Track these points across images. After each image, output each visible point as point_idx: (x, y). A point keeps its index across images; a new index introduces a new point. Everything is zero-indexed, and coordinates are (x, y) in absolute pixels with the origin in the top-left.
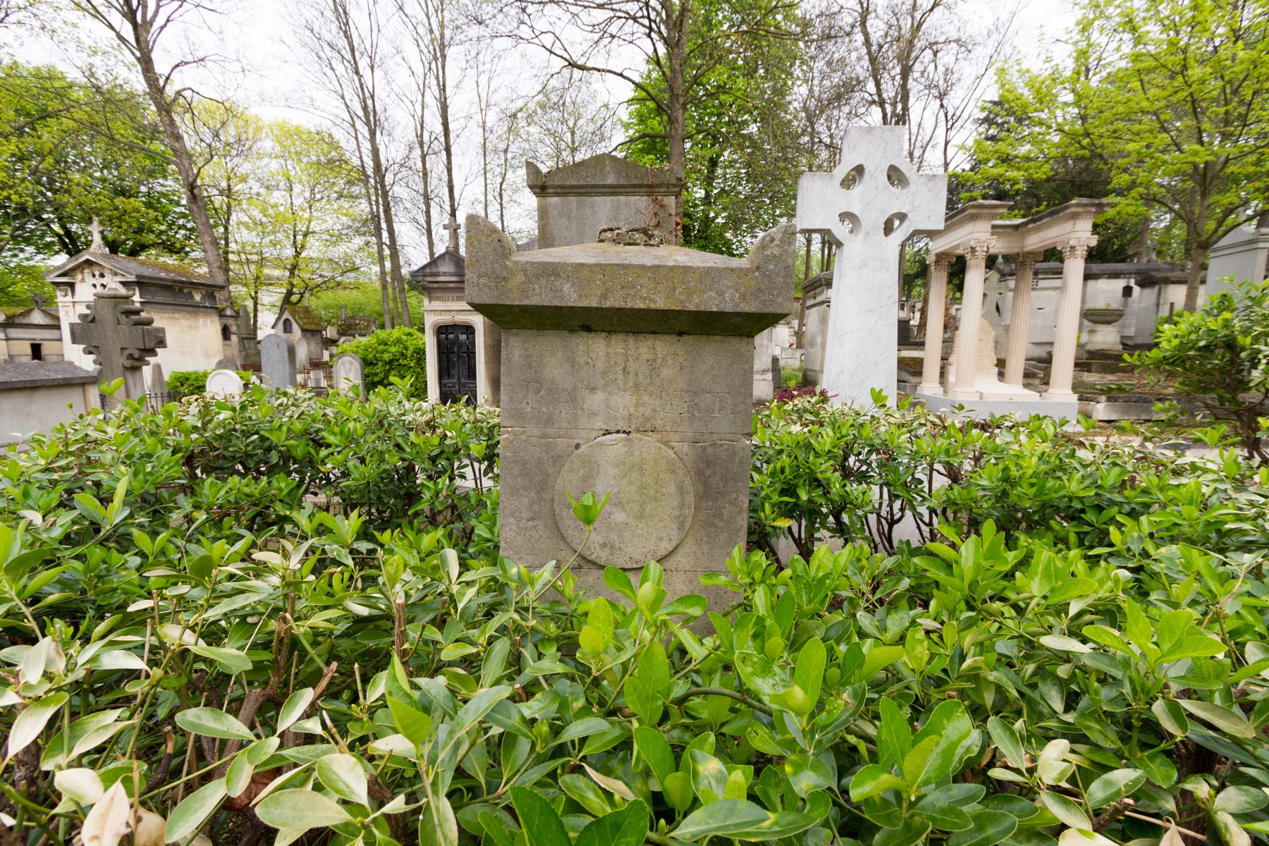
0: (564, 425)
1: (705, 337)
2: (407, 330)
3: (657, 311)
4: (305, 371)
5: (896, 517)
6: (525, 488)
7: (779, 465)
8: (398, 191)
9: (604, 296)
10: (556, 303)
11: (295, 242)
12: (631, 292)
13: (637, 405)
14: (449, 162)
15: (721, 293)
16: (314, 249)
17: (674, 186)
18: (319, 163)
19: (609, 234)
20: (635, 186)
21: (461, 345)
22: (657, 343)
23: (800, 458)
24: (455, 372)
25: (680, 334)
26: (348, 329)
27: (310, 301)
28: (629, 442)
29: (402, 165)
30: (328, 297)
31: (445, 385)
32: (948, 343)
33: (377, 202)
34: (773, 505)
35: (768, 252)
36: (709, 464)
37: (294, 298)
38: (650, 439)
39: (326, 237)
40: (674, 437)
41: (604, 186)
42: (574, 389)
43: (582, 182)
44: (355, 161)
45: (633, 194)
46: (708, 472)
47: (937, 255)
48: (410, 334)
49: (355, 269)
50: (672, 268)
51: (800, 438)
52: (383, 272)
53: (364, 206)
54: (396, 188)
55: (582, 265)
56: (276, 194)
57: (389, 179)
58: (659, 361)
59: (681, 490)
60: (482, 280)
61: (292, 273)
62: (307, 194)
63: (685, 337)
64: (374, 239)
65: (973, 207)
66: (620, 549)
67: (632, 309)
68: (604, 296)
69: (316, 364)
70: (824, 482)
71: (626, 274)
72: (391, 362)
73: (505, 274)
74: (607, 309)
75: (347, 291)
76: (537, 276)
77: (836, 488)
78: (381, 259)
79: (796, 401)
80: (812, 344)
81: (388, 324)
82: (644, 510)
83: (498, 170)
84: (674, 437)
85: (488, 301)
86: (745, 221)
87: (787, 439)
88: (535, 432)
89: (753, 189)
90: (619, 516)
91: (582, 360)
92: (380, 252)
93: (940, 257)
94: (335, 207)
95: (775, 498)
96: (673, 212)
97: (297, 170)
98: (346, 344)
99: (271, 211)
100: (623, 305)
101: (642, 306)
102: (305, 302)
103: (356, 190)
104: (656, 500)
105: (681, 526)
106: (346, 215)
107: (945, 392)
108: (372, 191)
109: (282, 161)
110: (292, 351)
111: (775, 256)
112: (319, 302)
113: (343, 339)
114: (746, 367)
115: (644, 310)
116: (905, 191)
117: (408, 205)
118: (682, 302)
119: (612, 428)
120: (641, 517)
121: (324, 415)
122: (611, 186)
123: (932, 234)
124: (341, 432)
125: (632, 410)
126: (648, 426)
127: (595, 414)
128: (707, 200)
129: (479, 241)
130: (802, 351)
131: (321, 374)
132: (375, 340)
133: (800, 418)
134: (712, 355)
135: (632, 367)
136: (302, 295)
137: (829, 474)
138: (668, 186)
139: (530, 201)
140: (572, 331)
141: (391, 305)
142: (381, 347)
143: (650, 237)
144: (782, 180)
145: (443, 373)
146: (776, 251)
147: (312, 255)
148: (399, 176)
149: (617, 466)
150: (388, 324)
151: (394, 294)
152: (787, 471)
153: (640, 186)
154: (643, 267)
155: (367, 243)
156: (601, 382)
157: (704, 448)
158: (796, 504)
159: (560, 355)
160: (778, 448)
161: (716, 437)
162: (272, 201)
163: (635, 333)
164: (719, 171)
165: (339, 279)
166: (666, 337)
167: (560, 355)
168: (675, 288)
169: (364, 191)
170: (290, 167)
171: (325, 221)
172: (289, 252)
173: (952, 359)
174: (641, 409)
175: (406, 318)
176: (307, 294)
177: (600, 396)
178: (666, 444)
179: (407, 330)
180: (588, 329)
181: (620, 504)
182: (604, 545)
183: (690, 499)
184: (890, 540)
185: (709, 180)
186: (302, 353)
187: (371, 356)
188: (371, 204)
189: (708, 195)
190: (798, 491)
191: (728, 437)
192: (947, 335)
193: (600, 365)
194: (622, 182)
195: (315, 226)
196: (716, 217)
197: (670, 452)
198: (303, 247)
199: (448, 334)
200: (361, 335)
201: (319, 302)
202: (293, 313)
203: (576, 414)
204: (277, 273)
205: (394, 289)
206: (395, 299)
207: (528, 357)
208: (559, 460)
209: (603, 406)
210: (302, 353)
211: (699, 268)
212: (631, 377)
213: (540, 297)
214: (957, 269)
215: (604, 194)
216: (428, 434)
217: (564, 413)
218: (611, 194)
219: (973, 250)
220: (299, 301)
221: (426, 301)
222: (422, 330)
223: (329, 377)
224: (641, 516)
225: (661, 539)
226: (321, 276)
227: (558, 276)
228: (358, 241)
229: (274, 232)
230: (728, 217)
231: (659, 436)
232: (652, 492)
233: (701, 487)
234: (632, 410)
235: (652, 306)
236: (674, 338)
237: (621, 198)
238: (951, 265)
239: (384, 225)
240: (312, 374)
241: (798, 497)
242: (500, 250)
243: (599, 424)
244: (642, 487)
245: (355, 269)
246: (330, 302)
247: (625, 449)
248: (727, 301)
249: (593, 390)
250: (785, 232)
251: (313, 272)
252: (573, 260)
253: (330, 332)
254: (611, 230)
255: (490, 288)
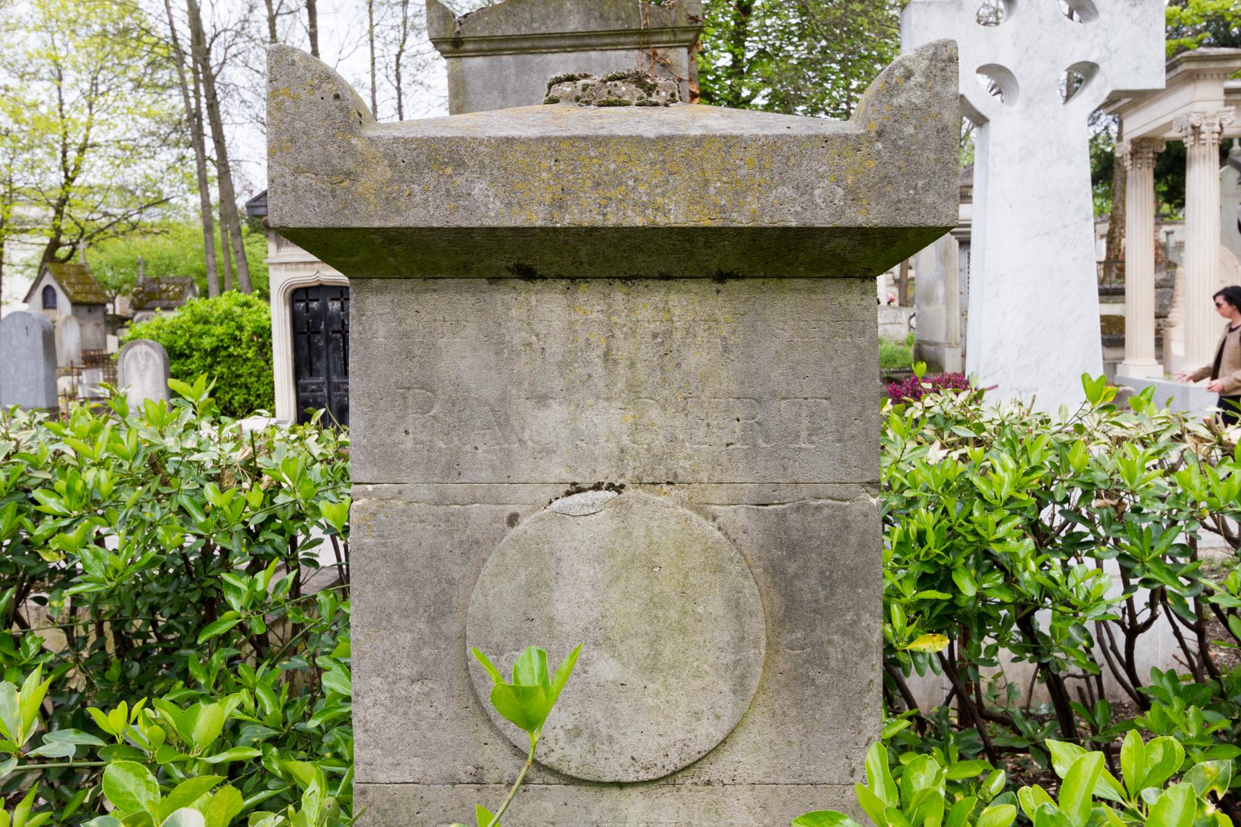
0: (485, 475)
1: (772, 283)
2: (242, 297)
3: (670, 231)
4: (71, 370)
5: (1142, 619)
6: (405, 613)
7: (913, 528)
8: (233, 75)
9: (559, 205)
10: (459, 221)
11: (64, 162)
12: (615, 193)
13: (636, 428)
14: (313, 24)
15: (804, 189)
16: (95, 172)
17: (685, 30)
18: (104, 34)
19: (567, 88)
20: (618, 33)
21: (330, 319)
22: (674, 298)
23: (953, 513)
24: (321, 365)
25: (721, 277)
26: (146, 300)
27: (88, 256)
28: (623, 509)
29: (238, 34)
30: (116, 248)
31: (305, 388)
32: (1165, 288)
33: (196, 91)
34: (906, 608)
35: (900, 100)
36: (793, 549)
37: (62, 252)
38: (664, 499)
39: (113, 151)
40: (717, 495)
41: (563, 36)
42: (503, 398)
43: (524, 31)
44: (163, 30)
45: (615, 47)
46: (792, 568)
47: (1133, 142)
48: (247, 304)
49: (161, 201)
50: (699, 141)
51: (951, 475)
52: (206, 205)
53: (175, 101)
54: (227, 70)
55: (509, 141)
56: (36, 86)
57: (215, 57)
58: (678, 335)
59: (736, 607)
60: (302, 179)
61: (59, 212)
62: (86, 86)
63: (732, 284)
64: (191, 153)
65: (1190, 59)
66: (610, 739)
67: (618, 229)
68: (559, 205)
69: (95, 359)
70: (1004, 560)
71: (604, 156)
72: (215, 351)
73: (350, 164)
74: (566, 230)
75: (149, 238)
76: (418, 168)
77: (1029, 573)
78: (203, 183)
79: (928, 401)
80: (928, 298)
81: (214, 288)
82: (658, 654)
83: (393, 34)
84: (717, 495)
85: (316, 222)
86: (802, 100)
87: (923, 476)
88: (424, 492)
89: (810, 49)
90: (606, 668)
91: (518, 338)
92: (202, 171)
93: (1139, 145)
94: (131, 104)
95: (911, 593)
96: (685, 75)
97: (73, 50)
98: (145, 324)
99: (27, 115)
100: (599, 221)
101: (639, 221)
102: (79, 258)
103: (163, 76)
104: (683, 631)
105: (740, 687)
106: (146, 115)
107: (1167, 372)
108: (189, 76)
109: (47, 37)
110: (49, 339)
111: (916, 108)
112: (103, 257)
113: (139, 315)
114: (863, 342)
115: (644, 229)
116: (1090, 25)
117: (248, 96)
118: (723, 210)
119: (586, 480)
120: (653, 669)
121: (58, 454)
122: (574, 35)
123: (1140, 98)
124: (69, 489)
125: (626, 440)
126: (661, 473)
127: (547, 451)
128: (736, 70)
129: (296, 100)
130: (910, 311)
131: (100, 375)
132: (188, 316)
133: (939, 433)
134: (789, 319)
135: (623, 349)
136: (74, 246)
137: (1012, 544)
138: (674, 30)
139: (439, 71)
140: (495, 279)
141: (220, 257)
142: (199, 328)
143: (650, 89)
144: (859, 34)
145: (302, 366)
146: (917, 97)
147: (92, 180)
148: (233, 50)
149: (598, 559)
150: (214, 288)
151: (224, 238)
152: (931, 538)
153: (625, 33)
154: (639, 141)
155: (182, 158)
156: (558, 384)
157: (782, 516)
158: (952, 604)
159: (470, 330)
160: (908, 494)
161: (805, 491)
162: (29, 98)
163: (627, 279)
164: (754, 24)
165: (135, 218)
166: (692, 285)
167: (470, 330)
168: (706, 183)
169: (176, 78)
170: (58, 44)
171: (112, 127)
172: (57, 178)
173: (1175, 315)
174: (645, 437)
175: (242, 277)
176: (82, 245)
177: (556, 413)
178: (699, 509)
179: (242, 297)
180: (528, 274)
181: (606, 642)
182: (575, 733)
183: (757, 627)
184: (1129, 665)
185: (738, 38)
186: (70, 340)
187: (181, 343)
188: (187, 97)
189: (736, 62)
190: (956, 578)
191: (830, 490)
192: (1163, 275)
193: (555, 348)
194: (594, 26)
195: (96, 135)
196: (753, 96)
197: (710, 526)
198: (77, 168)
199: (308, 301)
200: (165, 309)
201: (103, 257)
202: (58, 277)
203: (508, 453)
204: (34, 212)
205: (224, 231)
206: (225, 248)
207: (405, 335)
208: (474, 549)
209: (564, 433)
210: (70, 340)
211: (755, 139)
212: (622, 369)
213: (423, 210)
214: (1170, 166)
215: (563, 49)
216: (246, 485)
217: (481, 452)
218: (576, 48)
219: (1196, 130)
220: (69, 258)
221: (272, 247)
222: (266, 296)
223: (113, 380)
224: (652, 667)
225: (697, 716)
226: (106, 214)
227: (460, 165)
228: (167, 156)
229: (29, 148)
230: (774, 96)
231: (684, 494)
232: (673, 614)
233: (778, 600)
234: (626, 440)
235: (661, 221)
236: (709, 286)
237: (593, 54)
238: (1159, 157)
239: (207, 130)
240: (85, 376)
241: (955, 590)
242: (339, 116)
243: (558, 471)
244: (654, 603)
245: (161, 201)
246: (121, 256)
247: (614, 524)
248: (820, 204)
249: (542, 399)
250: (934, 58)
251: (94, 209)
252: (493, 133)
253: (120, 306)
254: (571, 79)
255: (318, 194)
